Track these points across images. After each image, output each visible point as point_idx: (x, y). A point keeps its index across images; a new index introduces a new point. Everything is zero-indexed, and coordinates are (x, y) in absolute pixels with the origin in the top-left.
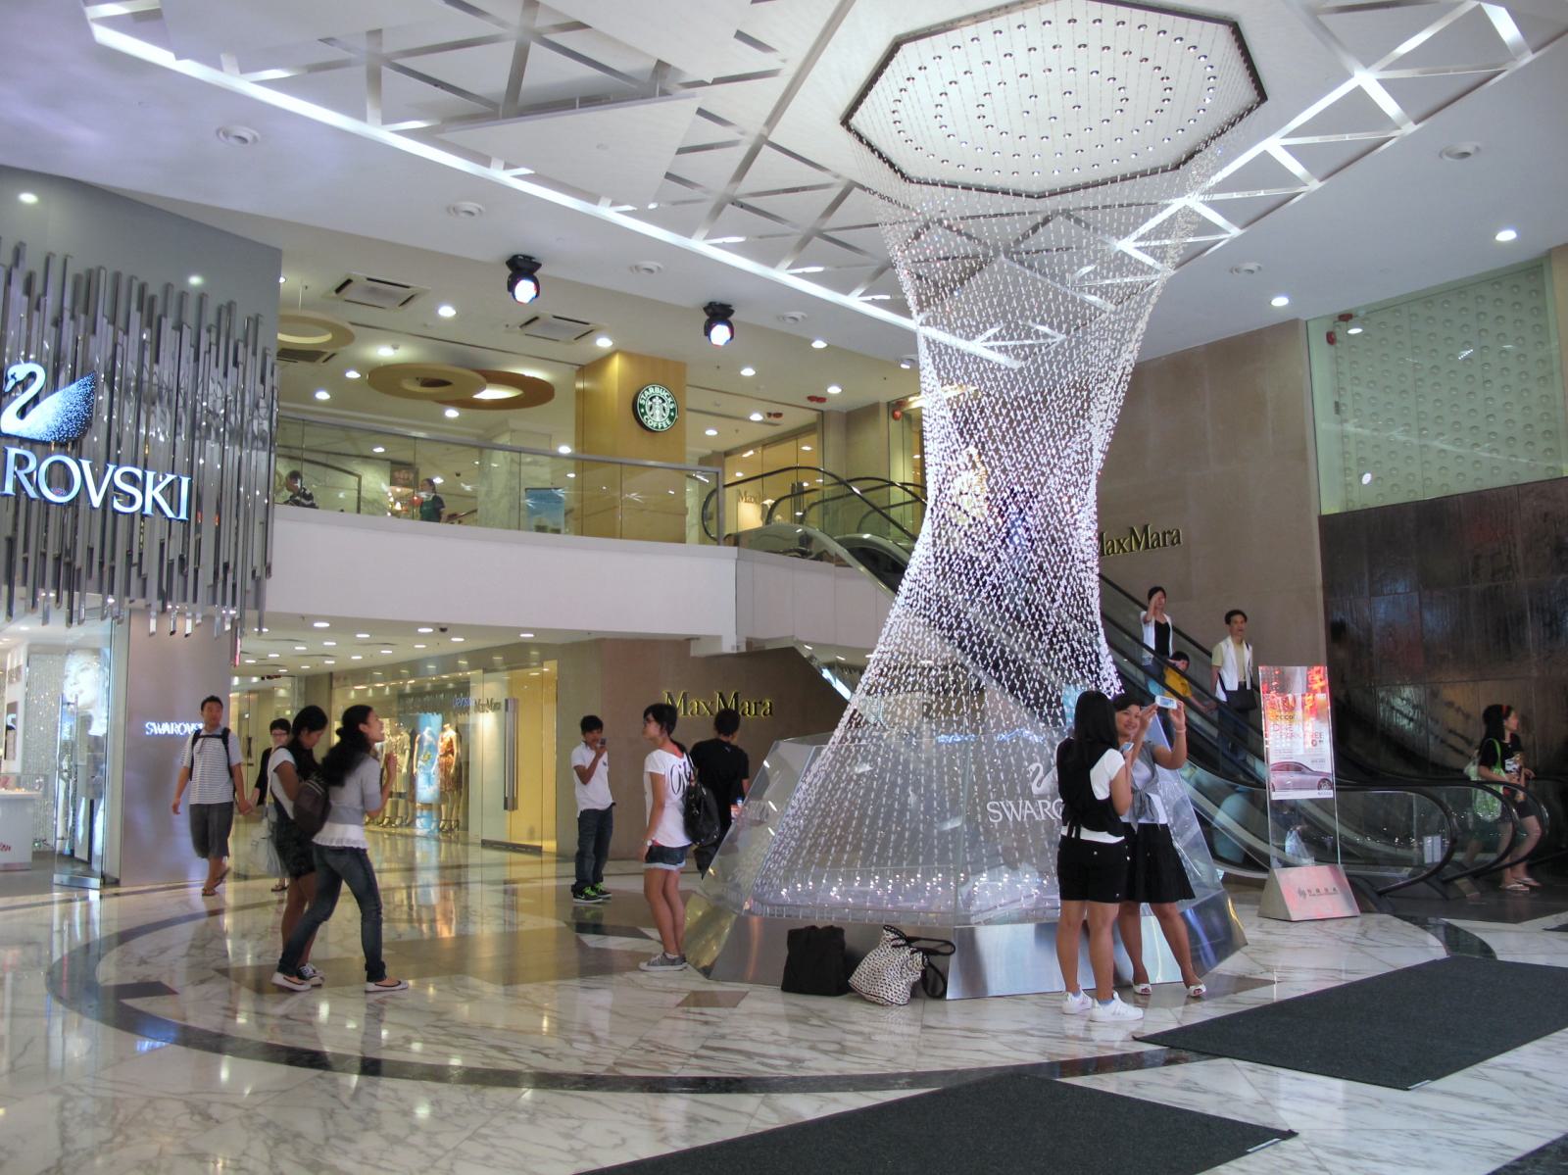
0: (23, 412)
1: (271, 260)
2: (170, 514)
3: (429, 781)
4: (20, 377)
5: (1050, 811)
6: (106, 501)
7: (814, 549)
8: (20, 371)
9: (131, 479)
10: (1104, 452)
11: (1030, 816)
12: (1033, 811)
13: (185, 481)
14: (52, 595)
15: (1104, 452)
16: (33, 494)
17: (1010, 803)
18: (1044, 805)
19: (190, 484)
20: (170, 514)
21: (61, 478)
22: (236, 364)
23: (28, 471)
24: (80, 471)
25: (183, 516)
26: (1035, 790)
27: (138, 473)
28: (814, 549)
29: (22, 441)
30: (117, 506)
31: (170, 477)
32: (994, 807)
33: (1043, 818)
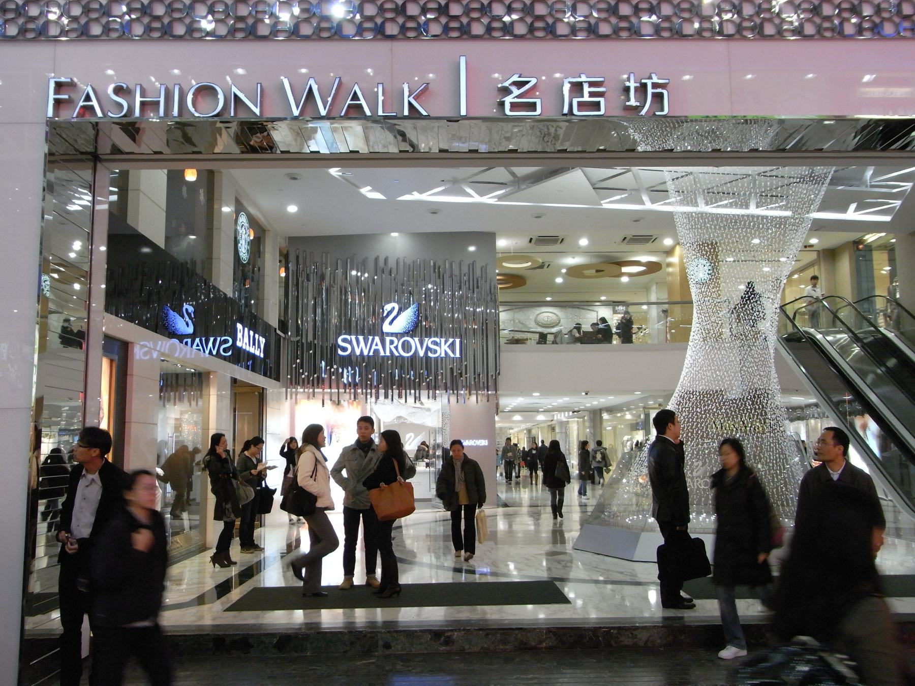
0: (391, 323)
1: (486, 239)
2: (452, 355)
3: (459, 612)
4: (389, 309)
5: (396, 348)
6: (426, 353)
7: (382, 500)
8: (388, 307)
9: (435, 343)
10: (533, 440)
11: (376, 351)
12: (380, 347)
13: (458, 341)
14: (311, 390)
15: (533, 440)
16: (396, 354)
17: (361, 338)
18: (392, 342)
19: (461, 342)
20: (452, 355)
21: (406, 347)
22: (478, 287)
23: (395, 344)
24: (414, 342)
25: (458, 355)
26: (386, 328)
27: (437, 340)
28: (382, 500)
29: (392, 334)
30: (430, 354)
31: (451, 340)
32: (344, 340)
33: (388, 354)
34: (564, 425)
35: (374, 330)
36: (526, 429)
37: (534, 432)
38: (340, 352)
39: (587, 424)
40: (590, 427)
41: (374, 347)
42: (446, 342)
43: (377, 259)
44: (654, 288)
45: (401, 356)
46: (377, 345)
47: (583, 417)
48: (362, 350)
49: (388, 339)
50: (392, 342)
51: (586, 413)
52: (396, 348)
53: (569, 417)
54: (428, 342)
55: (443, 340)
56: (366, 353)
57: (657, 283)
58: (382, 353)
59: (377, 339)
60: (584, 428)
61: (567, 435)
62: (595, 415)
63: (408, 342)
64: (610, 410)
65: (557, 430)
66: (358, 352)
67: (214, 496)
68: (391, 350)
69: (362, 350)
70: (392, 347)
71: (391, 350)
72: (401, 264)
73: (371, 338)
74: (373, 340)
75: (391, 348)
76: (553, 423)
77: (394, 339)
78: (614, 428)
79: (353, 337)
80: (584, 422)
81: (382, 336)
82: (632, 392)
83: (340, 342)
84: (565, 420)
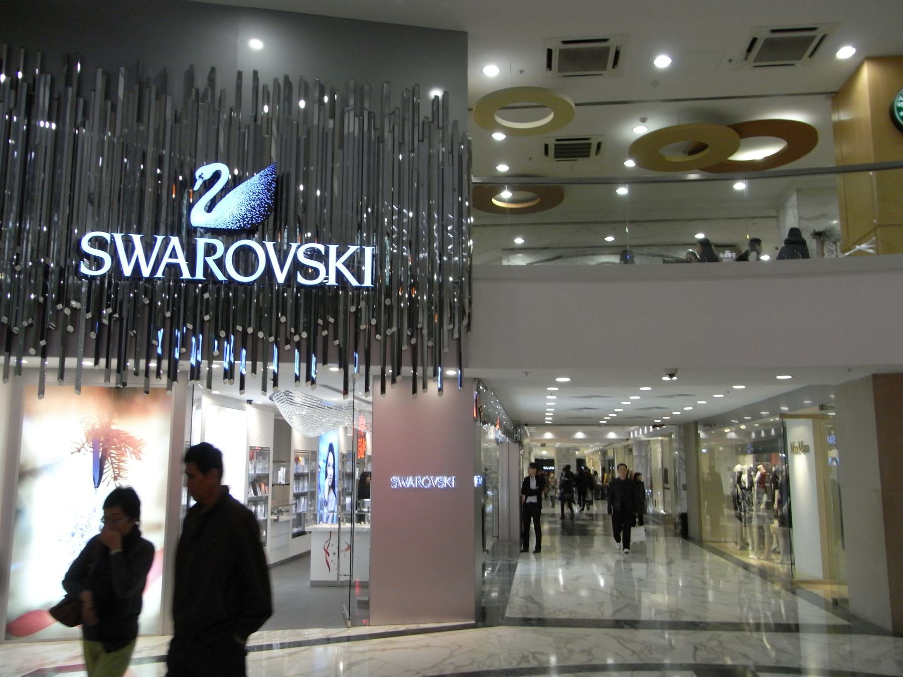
0: (210, 208)
2: (354, 282)
5: (220, 263)
6: (291, 277)
8: (205, 171)
9: (314, 254)
11: (173, 269)
13: (369, 251)
16: (220, 276)
17: (136, 238)
18: (210, 250)
20: (354, 282)
21: (245, 260)
24: (264, 251)
25: (368, 282)
26: (199, 217)
29: (215, 232)
31: (352, 249)
32: (100, 243)
33: (199, 275)
34: (644, 445)
35: (166, 215)
36: (600, 450)
37: (610, 454)
38: (84, 269)
39: (675, 445)
40: (679, 450)
41: (166, 260)
42: (339, 255)
43: (190, 76)
44: (793, 200)
45: (231, 280)
46: (173, 255)
47: (669, 435)
48: (137, 268)
49: (201, 243)
50: (210, 250)
51: (674, 429)
52: (220, 263)
53: (649, 434)
54: (299, 251)
55: (333, 249)
56: (146, 272)
57: (798, 191)
58: (186, 275)
59: (175, 241)
60: (672, 450)
61: (647, 459)
62: (688, 430)
63: (249, 250)
64: (713, 423)
65: (635, 453)
66: (127, 270)
67: (147, 535)
68: (206, 265)
69: (137, 268)
70: (210, 260)
71: (206, 265)
72: (248, 81)
73: (160, 238)
74: (166, 243)
75: (219, 262)
76: (630, 442)
77: (219, 244)
78: (711, 451)
79: (118, 237)
80: (671, 441)
81: (189, 235)
82: (766, 374)
83: (85, 246)
84: (644, 439)
